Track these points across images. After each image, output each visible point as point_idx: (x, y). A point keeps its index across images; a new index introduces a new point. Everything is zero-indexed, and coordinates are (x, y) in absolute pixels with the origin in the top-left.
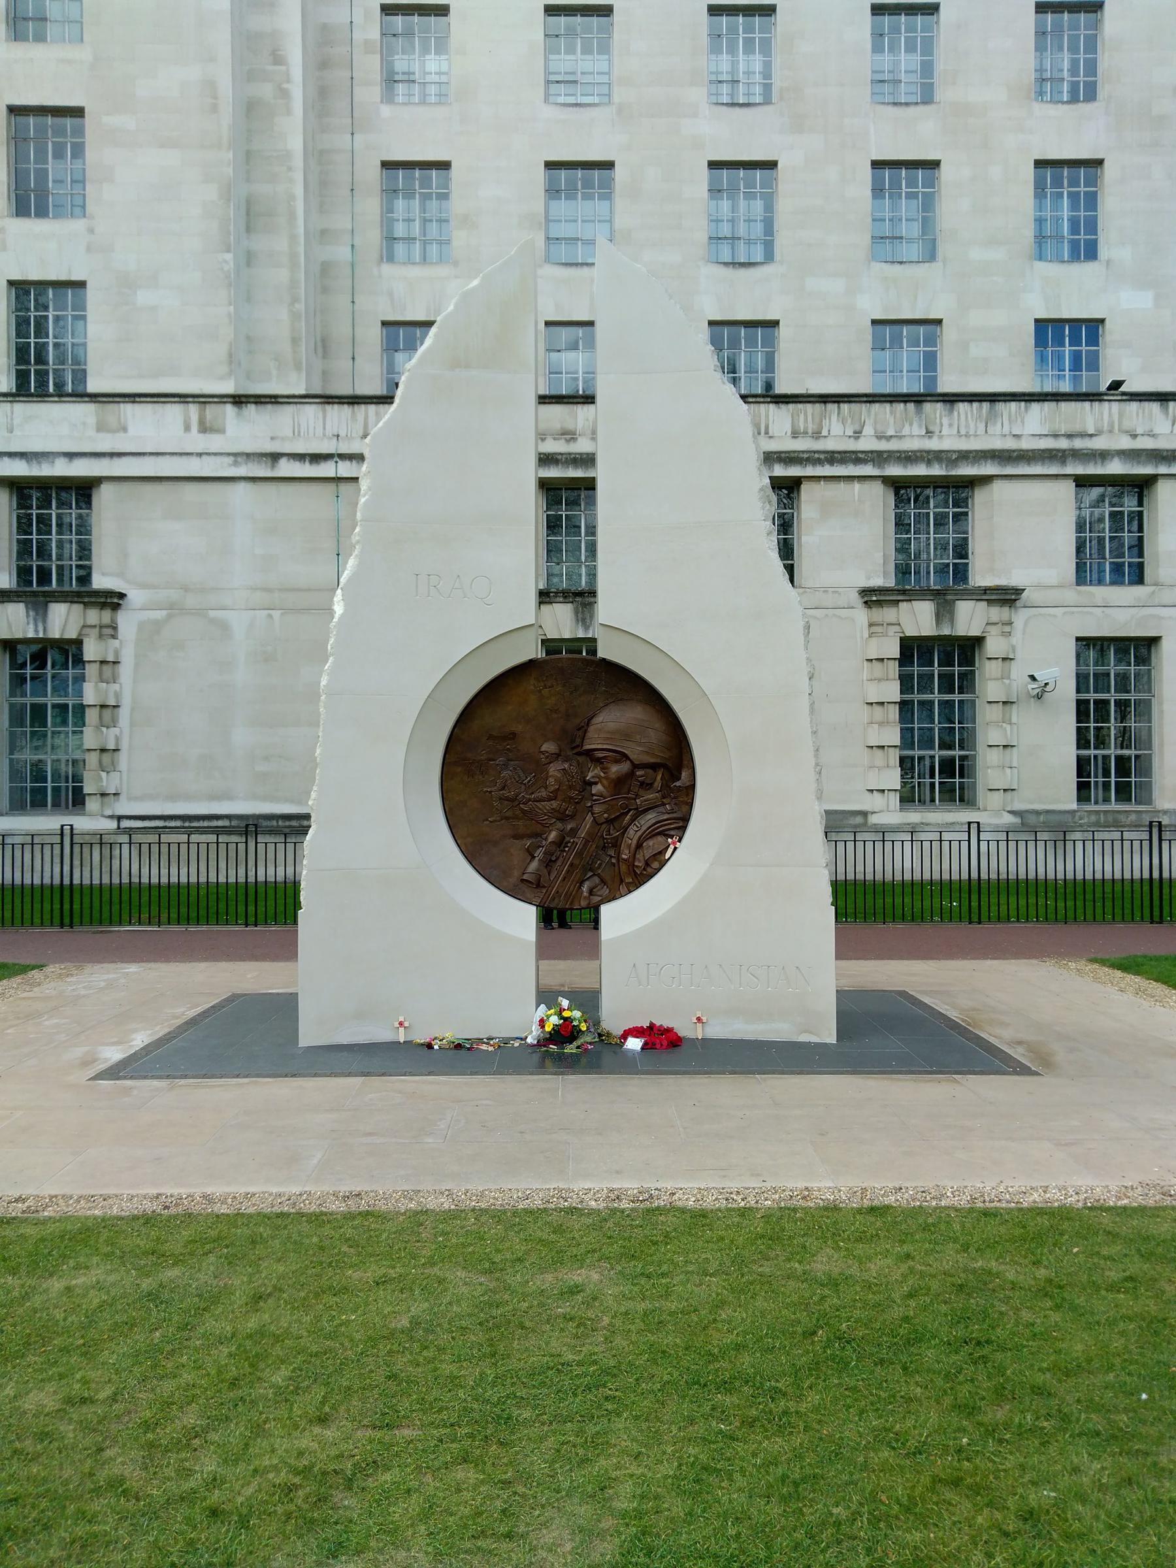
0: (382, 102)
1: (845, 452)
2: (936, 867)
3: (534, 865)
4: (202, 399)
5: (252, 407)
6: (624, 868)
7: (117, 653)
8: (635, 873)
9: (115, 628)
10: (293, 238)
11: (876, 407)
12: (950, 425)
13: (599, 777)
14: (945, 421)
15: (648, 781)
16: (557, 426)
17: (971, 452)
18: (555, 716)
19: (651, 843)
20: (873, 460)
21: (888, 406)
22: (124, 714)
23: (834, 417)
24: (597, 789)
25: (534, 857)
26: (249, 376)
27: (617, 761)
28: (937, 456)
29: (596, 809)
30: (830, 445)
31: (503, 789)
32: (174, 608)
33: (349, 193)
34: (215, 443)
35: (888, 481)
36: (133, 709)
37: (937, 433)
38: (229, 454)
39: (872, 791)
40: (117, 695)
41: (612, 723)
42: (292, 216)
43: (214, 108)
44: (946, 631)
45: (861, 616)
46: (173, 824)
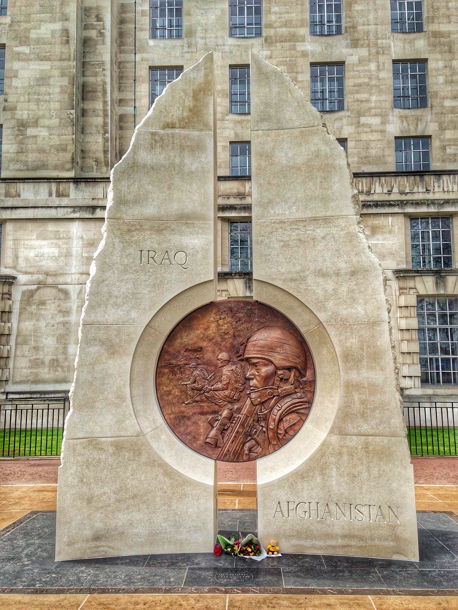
0: (150, 38)
1: (383, 201)
2: (445, 419)
3: (213, 432)
4: (58, 180)
5: (83, 184)
6: (271, 434)
7: (10, 307)
9: (10, 295)
10: (105, 102)
11: (399, 179)
12: (439, 187)
14: (436, 185)
15: (285, 378)
17: (451, 200)
18: (227, 336)
19: (288, 418)
20: (398, 205)
21: (405, 178)
22: (13, 339)
23: (377, 184)
24: (253, 382)
25: (213, 427)
26: (82, 169)
27: (265, 365)
28: (433, 202)
29: (253, 395)
30: (376, 198)
31: (194, 382)
32: (41, 285)
33: (133, 82)
34: (65, 201)
35: (406, 215)
36: (17, 336)
37: (432, 191)
38: (71, 207)
39: (405, 377)
40: (10, 329)
42: (105, 92)
43: (67, 42)
44: (442, 292)
45: (394, 285)
46: (35, 396)
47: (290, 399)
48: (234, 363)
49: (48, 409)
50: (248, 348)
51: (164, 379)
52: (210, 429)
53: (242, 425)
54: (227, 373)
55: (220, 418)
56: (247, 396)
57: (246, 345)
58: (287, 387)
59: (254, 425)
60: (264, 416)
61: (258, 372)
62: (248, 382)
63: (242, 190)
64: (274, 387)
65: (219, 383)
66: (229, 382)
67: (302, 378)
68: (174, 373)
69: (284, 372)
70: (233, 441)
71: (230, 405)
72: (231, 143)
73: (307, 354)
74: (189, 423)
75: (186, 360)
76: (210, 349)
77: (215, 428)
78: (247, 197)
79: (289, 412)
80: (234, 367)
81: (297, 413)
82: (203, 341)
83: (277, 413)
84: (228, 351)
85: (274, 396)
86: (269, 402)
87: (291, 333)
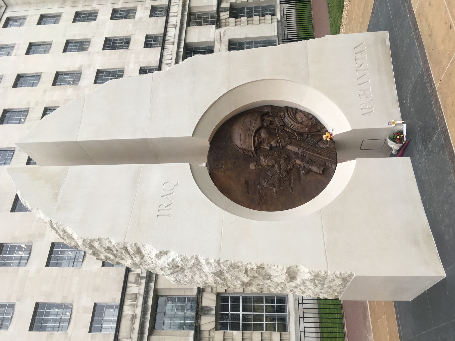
3: (315, 169)
13: (268, 143)
18: (237, 164)
27: (260, 135)
29: (284, 144)
31: (274, 185)
41: (241, 139)
49: (304, 318)
53: (308, 149)
63: (130, 317)
81: (295, 114)
84: (249, 163)
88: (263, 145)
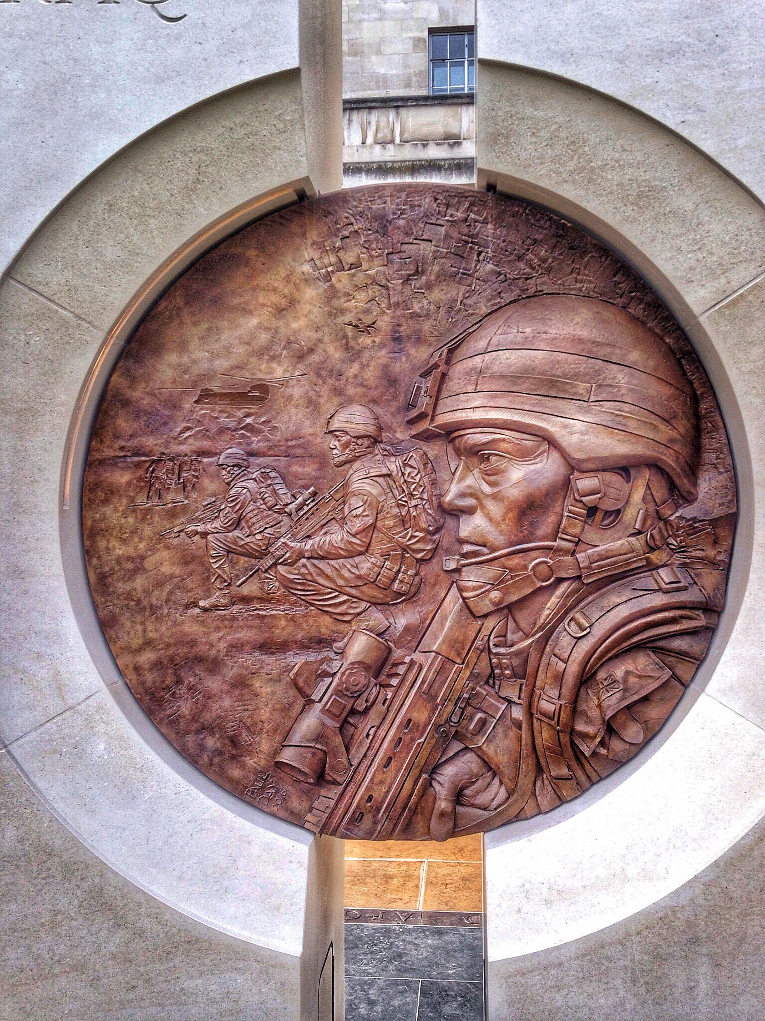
3: (309, 723)
8: (578, 755)
15: (608, 505)
16: (440, 129)
19: (619, 671)
24: (472, 526)
25: (309, 702)
27: (524, 455)
29: (472, 578)
31: (237, 524)
47: (627, 594)
48: (396, 450)
50: (453, 385)
51: (113, 514)
52: (298, 707)
54: (368, 487)
55: (336, 665)
56: (445, 580)
57: (444, 375)
58: (613, 543)
59: (475, 696)
60: (516, 662)
61: (491, 484)
62: (450, 522)
64: (558, 543)
65: (334, 527)
66: (373, 526)
67: (677, 507)
68: (149, 485)
69: (603, 482)
70: (390, 759)
71: (379, 615)
72: (432, 31)
73: (704, 407)
74: (214, 684)
75: (204, 434)
76: (297, 392)
77: (318, 706)
78: (464, 143)
79: (624, 645)
80: (393, 465)
81: (657, 650)
82: (273, 358)
83: (572, 650)
85: (560, 581)
86: (540, 599)
87: (635, 319)
88: (468, 468)
